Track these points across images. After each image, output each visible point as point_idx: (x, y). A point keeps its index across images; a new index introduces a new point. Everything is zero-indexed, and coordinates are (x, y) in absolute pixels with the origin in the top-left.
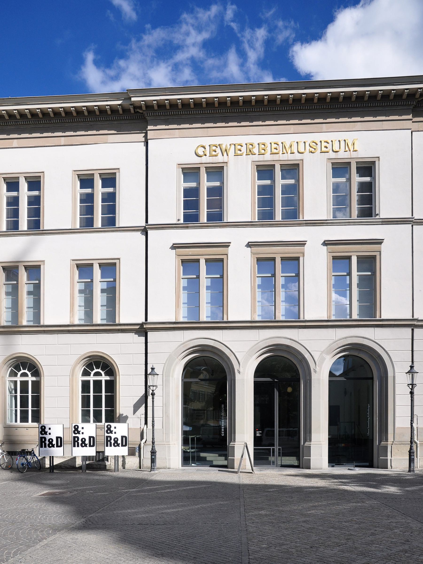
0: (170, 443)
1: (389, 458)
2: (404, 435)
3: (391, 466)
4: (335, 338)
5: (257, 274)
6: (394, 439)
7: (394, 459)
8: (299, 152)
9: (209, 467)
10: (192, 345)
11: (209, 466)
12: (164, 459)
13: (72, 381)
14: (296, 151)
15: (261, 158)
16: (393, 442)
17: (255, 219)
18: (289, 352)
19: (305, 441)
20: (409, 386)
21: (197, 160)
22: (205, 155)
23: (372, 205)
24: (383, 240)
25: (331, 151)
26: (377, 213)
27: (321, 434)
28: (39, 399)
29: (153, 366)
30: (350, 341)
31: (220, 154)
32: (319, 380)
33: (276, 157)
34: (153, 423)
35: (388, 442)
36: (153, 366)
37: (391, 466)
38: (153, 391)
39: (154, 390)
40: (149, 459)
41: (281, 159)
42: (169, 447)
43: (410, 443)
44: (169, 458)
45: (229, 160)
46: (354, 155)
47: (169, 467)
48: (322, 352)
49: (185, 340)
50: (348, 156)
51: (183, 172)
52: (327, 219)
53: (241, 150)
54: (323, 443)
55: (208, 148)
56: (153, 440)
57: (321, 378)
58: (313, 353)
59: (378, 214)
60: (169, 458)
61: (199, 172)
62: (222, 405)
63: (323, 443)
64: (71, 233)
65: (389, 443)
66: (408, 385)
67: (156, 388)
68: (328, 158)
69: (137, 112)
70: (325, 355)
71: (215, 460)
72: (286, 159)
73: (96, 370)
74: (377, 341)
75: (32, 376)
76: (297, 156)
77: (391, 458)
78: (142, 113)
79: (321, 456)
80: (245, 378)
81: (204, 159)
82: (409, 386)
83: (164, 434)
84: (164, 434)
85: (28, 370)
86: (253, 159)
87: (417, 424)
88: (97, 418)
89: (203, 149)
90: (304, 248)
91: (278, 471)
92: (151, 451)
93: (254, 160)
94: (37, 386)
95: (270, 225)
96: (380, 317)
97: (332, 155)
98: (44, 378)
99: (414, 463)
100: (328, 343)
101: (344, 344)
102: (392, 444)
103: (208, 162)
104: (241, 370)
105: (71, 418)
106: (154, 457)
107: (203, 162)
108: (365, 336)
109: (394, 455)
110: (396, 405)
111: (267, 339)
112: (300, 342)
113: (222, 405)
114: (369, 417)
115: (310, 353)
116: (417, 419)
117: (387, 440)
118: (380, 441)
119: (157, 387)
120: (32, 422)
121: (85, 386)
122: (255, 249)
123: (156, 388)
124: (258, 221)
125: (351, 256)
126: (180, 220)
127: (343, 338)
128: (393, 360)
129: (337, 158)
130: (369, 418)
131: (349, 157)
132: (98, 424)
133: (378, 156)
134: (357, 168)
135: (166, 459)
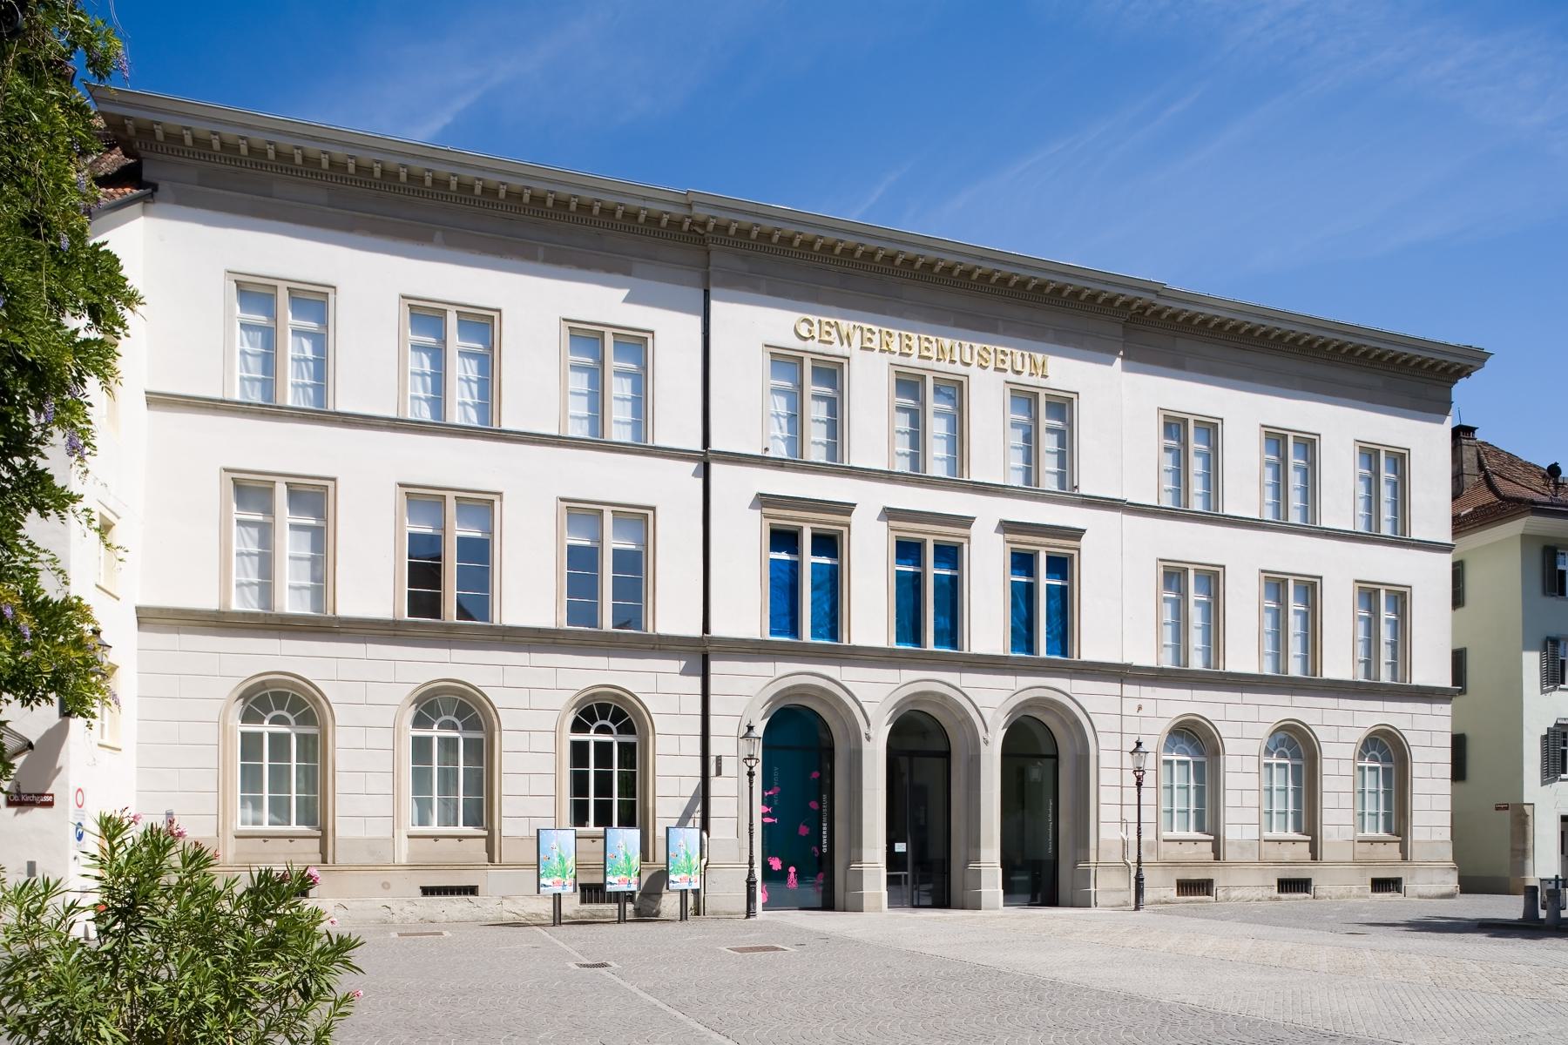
0: (863, 865)
1: (1092, 889)
5: (407, 525)
6: (1098, 859)
8: (802, 337)
13: (396, 739)
14: (957, 358)
18: (823, 702)
21: (800, 345)
22: (813, 337)
24: (855, 505)
25: (958, 363)
31: (837, 342)
40: (549, 898)
43: (748, 866)
49: (777, 676)
51: (293, 298)
53: (1466, 423)
61: (444, 319)
64: (196, 406)
69: (694, 230)
71: (1450, 896)
73: (600, 722)
75: (297, 724)
78: (703, 235)
81: (812, 345)
85: (456, 716)
88: (604, 819)
94: (628, 751)
96: (1079, 658)
98: (500, 735)
99: (755, 901)
103: (817, 350)
105: (557, 816)
107: (809, 349)
117: (1087, 860)
118: (848, 866)
120: (596, 825)
121: (579, 750)
128: (1097, 729)
132: (578, 829)
133: (1076, 391)
134: (1047, 403)
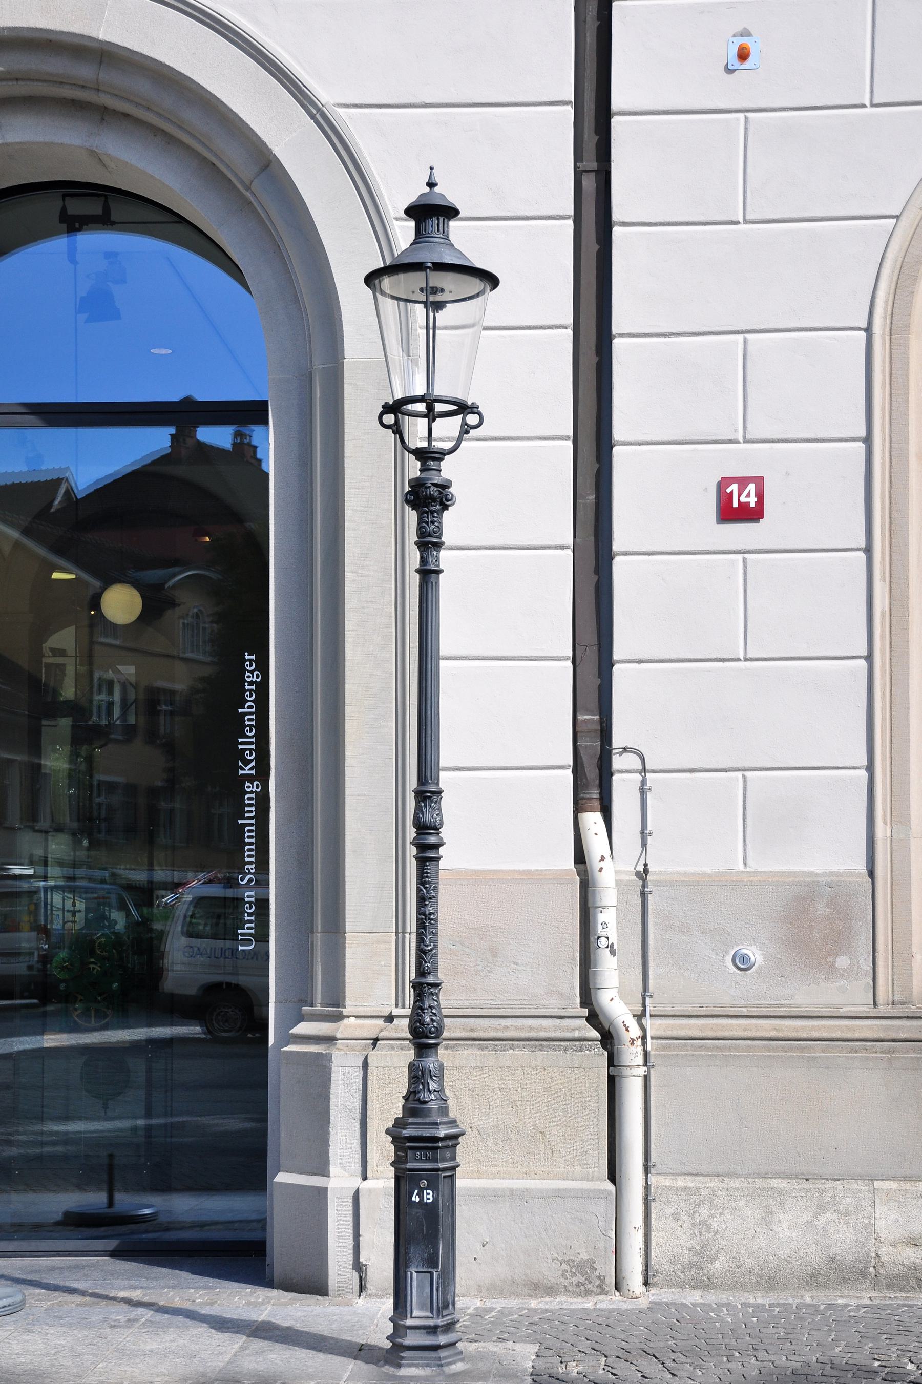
2: (495, 955)
3: (359, 1267)
9: (115, 1254)
11: (112, 1244)
20: (397, 430)
29: (431, 185)
34: (427, 818)
36: (431, 185)
37: (359, 1267)
38: (426, 456)
39: (441, 455)
56: (418, 1009)
65: (348, 1027)
66: (389, 419)
67: (466, 429)
77: (357, 1182)
82: (397, 430)
87: (644, 835)
92: (399, 1123)
106: (429, 1196)
116: (643, 791)
119: (472, 419)
123: (466, 429)
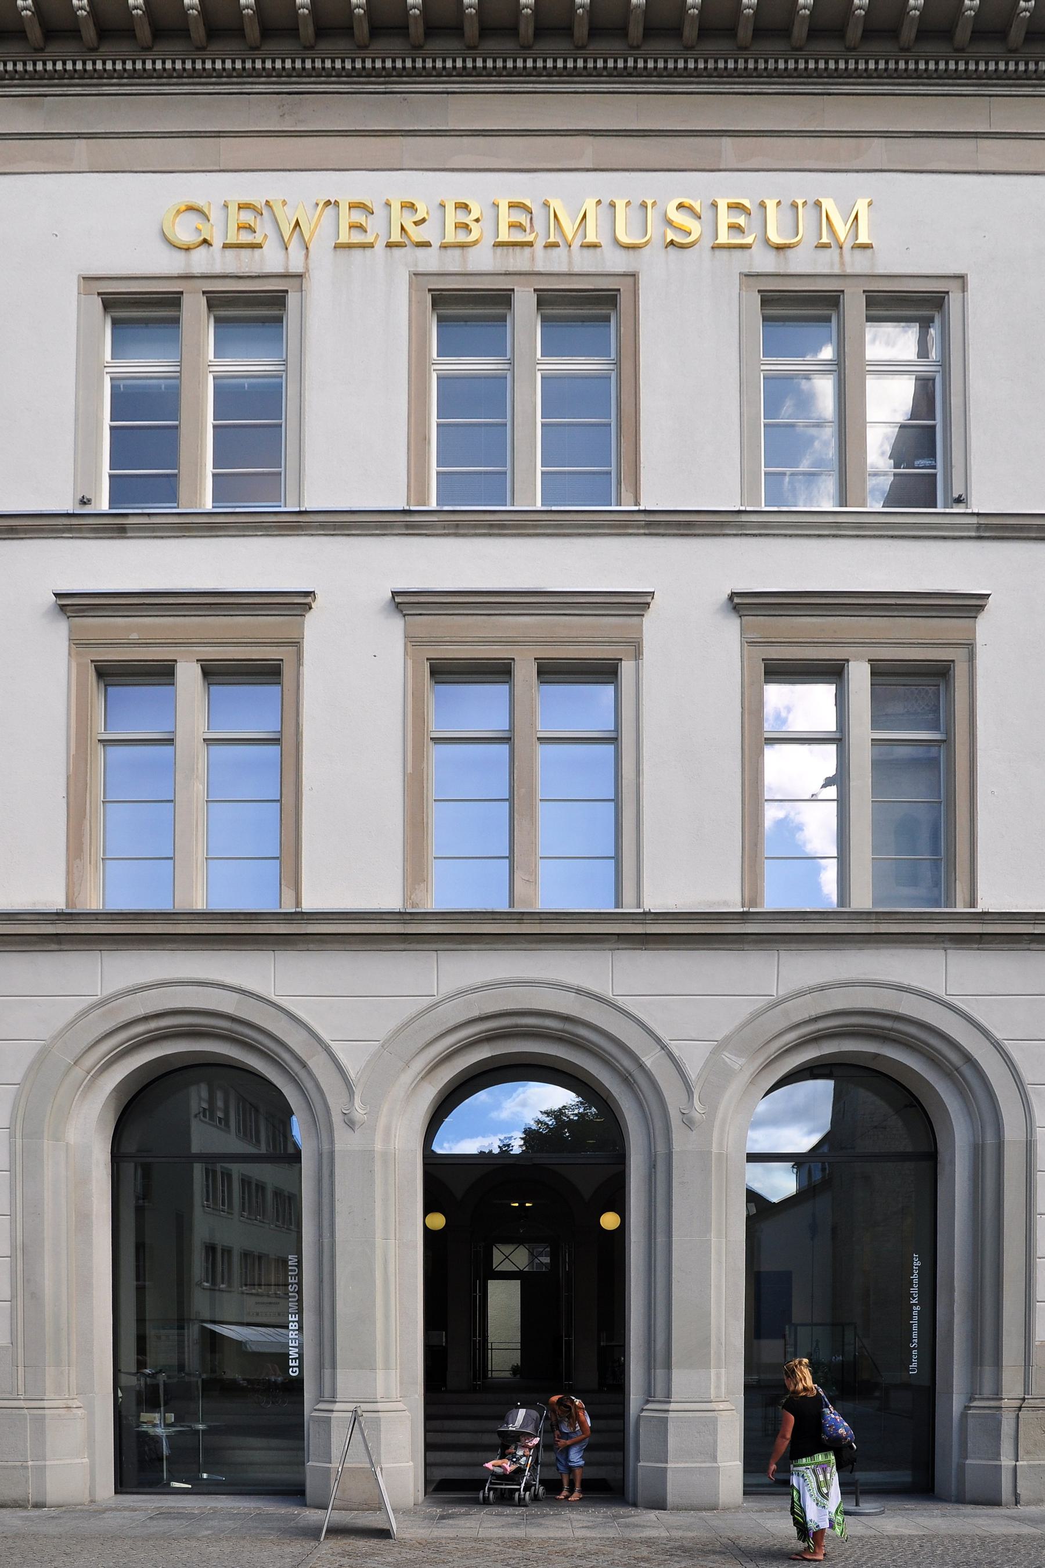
0: (379, 1406)
1: (1006, 1461)
4: (775, 990)
6: (1027, 1389)
7: (1030, 1466)
10: (141, 1012)
12: (14, 1467)
15: (452, 262)
16: (1024, 1399)
17: (423, 499)
19: (649, 1396)
21: (169, 263)
23: (934, 420)
26: (956, 496)
27: (713, 1371)
28: (624, 1370)
30: (840, 1001)
32: (705, 1156)
33: (518, 261)
35: (1002, 1399)
41: (540, 267)
42: (40, 1422)
44: (39, 1463)
45: (311, 266)
46: (857, 264)
47: (40, 1499)
48: (722, 1045)
50: (832, 265)
52: (742, 508)
54: (722, 1406)
55: (215, 214)
57: (715, 1149)
58: (676, 1046)
59: (960, 496)
60: (39, 1463)
62: (290, 1257)
63: (722, 1406)
65: (1005, 1403)
68: (746, 270)
70: (733, 1057)
72: (564, 269)
74: (959, 1000)
76: (615, 262)
79: (714, 1459)
80: (378, 1146)
81: (200, 262)
83: (21, 1369)
84: (21, 1369)
86: (416, 265)
89: (194, 219)
90: (642, 625)
91: (515, 1520)
93: (421, 269)
95: (491, 526)
97: (765, 262)
100: (746, 1008)
101: (814, 1013)
102: (1020, 1408)
103: (218, 269)
104: (359, 1111)
107: (197, 270)
108: (906, 981)
109: (1028, 1453)
110: (1039, 1254)
111: (475, 990)
112: (620, 1001)
113: (290, 1257)
114: (916, 1305)
115: (664, 1047)
122: (424, 624)
124: (438, 508)
125: (848, 661)
126: (89, 500)
127: (812, 990)
128: (1027, 1077)
129: (782, 271)
130: (918, 1308)
131: (837, 271)
135: (27, 1467)
